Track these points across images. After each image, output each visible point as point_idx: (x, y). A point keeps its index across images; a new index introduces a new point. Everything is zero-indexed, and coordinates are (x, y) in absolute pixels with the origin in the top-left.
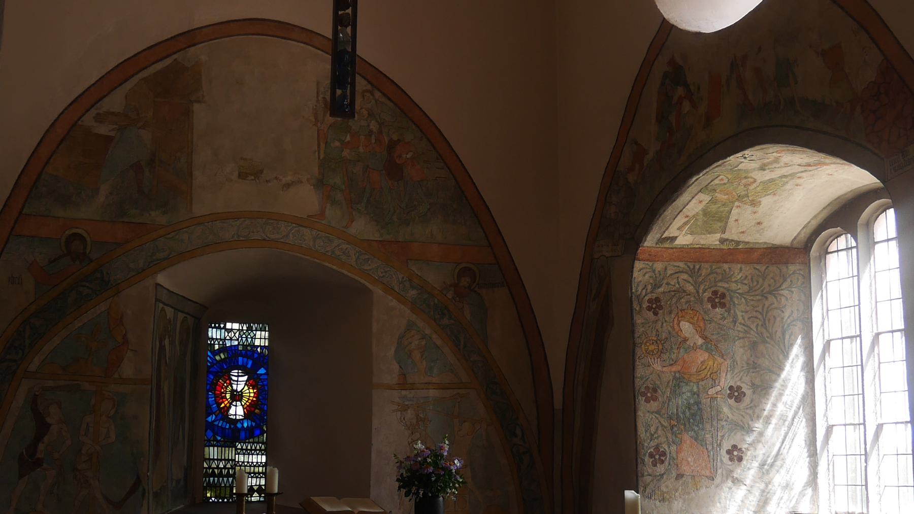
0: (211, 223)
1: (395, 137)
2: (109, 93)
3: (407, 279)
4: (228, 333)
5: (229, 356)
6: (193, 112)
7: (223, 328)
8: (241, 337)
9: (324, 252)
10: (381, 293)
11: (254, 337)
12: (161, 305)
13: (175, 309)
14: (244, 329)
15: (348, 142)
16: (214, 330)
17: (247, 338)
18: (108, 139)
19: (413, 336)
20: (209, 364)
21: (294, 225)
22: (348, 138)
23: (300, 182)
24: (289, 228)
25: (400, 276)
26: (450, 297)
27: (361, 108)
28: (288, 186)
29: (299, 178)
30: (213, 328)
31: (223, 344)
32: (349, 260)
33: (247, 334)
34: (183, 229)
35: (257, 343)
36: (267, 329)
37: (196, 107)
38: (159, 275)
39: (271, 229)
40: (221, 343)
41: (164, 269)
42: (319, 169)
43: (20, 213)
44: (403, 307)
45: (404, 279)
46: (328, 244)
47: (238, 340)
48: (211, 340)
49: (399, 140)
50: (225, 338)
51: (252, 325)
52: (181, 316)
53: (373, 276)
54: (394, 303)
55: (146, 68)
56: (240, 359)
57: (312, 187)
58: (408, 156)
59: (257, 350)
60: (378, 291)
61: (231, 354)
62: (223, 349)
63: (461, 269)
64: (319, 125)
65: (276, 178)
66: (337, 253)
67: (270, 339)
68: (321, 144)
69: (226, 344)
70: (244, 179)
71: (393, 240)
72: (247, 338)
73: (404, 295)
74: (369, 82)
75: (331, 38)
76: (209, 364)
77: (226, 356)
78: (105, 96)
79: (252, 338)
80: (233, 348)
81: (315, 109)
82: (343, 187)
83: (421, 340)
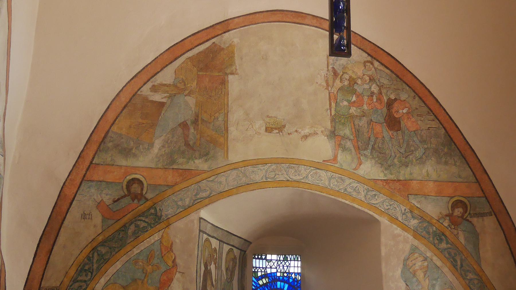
0: (244, 168)
1: (393, 97)
2: (162, 69)
3: (409, 211)
4: (269, 263)
5: (270, 281)
6: (228, 81)
7: (264, 259)
8: (279, 265)
9: (338, 190)
10: (387, 222)
11: (289, 266)
12: (205, 236)
13: (220, 241)
14: (281, 259)
15: (354, 102)
16: (258, 260)
17: (283, 266)
18: (162, 105)
19: (416, 258)
20: (254, 288)
21: (312, 168)
22: (354, 99)
23: (316, 134)
24: (308, 171)
25: (403, 208)
26: (446, 225)
27: (364, 75)
28: (306, 137)
29: (315, 131)
30: (256, 259)
31: (265, 272)
32: (359, 196)
33: (283, 263)
34: (221, 173)
35: (292, 270)
36: (299, 259)
37: (230, 77)
38: (202, 211)
39: (293, 172)
40: (263, 270)
41: (206, 206)
42: (331, 123)
43: (91, 163)
44: (406, 234)
45: (407, 211)
46: (341, 184)
47: (276, 268)
48: (255, 268)
49: (396, 99)
50: (266, 267)
51: (287, 256)
52: (226, 248)
53: (380, 208)
54: (398, 231)
55: (191, 49)
56: (279, 283)
57: (326, 138)
58: (405, 111)
59: (291, 276)
60: (384, 221)
61: (271, 279)
62: (265, 276)
63: (453, 202)
64: (330, 89)
65: (296, 131)
66: (349, 190)
67: (302, 267)
68: (332, 103)
69: (267, 272)
70: (270, 133)
71: (395, 179)
72: (283, 266)
73: (407, 224)
74: (369, 55)
75: (328, 19)
76: (254, 288)
77: (267, 281)
78: (158, 72)
79: (287, 266)
80: (273, 275)
81: (327, 77)
82: (352, 137)
83: (423, 262)
